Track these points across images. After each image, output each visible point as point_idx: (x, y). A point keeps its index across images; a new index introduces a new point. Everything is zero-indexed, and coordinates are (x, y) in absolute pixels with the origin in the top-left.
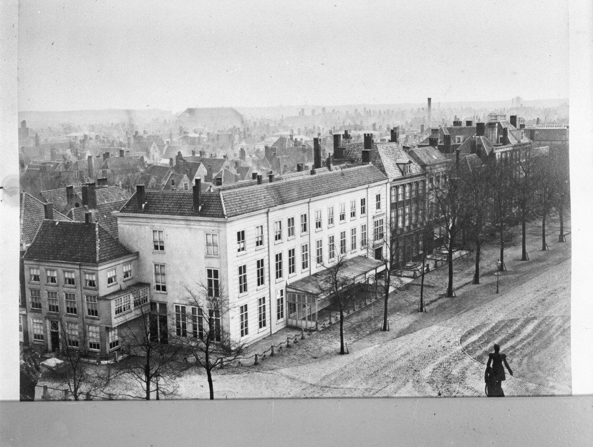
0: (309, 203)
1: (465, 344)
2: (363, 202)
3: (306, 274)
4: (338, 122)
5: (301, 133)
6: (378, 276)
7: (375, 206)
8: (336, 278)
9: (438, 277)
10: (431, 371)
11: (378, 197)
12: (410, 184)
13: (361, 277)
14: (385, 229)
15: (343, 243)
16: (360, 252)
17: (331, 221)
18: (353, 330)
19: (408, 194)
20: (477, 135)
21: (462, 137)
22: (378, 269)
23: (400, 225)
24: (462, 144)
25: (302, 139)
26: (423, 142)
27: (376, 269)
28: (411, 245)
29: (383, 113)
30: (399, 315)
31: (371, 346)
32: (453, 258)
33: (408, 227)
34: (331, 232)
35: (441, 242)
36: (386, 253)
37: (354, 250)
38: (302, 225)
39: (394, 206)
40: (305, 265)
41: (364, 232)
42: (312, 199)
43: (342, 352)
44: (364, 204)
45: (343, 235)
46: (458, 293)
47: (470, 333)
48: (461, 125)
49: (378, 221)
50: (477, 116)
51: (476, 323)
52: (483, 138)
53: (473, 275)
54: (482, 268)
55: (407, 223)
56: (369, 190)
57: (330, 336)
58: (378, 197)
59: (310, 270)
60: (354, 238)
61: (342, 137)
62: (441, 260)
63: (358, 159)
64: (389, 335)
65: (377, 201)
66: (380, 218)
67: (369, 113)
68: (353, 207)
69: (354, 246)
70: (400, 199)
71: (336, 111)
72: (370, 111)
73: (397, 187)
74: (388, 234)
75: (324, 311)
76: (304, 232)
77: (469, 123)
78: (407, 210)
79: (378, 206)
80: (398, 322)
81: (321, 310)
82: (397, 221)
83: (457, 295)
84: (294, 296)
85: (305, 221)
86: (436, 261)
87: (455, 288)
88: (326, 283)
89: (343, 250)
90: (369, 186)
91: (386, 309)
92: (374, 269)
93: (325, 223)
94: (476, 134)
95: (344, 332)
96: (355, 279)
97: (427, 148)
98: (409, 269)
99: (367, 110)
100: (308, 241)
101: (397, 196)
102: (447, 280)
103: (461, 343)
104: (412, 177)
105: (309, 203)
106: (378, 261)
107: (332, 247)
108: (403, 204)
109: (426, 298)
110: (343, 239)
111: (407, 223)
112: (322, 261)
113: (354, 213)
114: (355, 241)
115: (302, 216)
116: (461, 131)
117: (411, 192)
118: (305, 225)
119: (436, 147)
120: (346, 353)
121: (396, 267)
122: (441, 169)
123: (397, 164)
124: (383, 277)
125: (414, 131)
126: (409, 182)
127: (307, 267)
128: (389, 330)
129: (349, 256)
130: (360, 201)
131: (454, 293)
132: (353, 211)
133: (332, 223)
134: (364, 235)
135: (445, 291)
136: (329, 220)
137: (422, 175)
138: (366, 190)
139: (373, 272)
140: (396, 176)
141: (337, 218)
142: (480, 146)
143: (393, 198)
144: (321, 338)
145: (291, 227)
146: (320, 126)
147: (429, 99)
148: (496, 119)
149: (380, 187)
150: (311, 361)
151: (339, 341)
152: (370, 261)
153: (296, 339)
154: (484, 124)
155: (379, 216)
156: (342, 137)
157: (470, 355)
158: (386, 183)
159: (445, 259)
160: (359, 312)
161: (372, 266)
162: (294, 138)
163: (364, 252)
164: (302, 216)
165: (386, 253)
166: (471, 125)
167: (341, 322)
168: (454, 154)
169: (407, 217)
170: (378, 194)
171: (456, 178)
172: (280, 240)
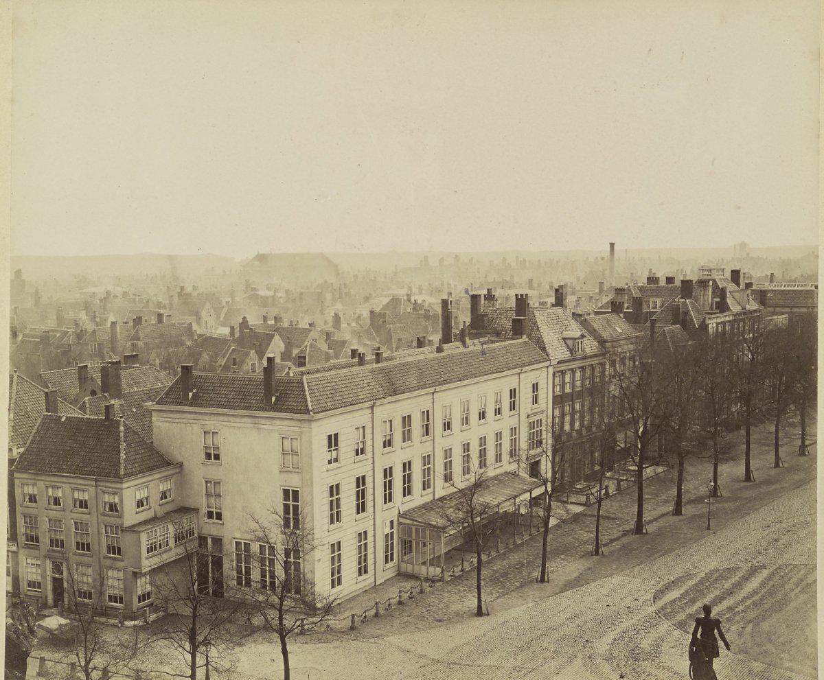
0: (433, 393)
1: (660, 604)
2: (513, 393)
3: (429, 498)
5: (423, 292)
6: (534, 502)
8: (471, 504)
10: (610, 642)
11: (535, 387)
12: (582, 368)
16: (507, 466)
17: (466, 420)
18: (496, 580)
19: (578, 383)
21: (659, 301)
23: (567, 427)
27: (530, 491)
34: (482, 431)
35: (626, 453)
39: (559, 400)
40: (426, 485)
42: (439, 388)
43: (480, 613)
45: (483, 441)
46: (650, 529)
47: (668, 588)
49: (534, 422)
51: (677, 572)
52: (691, 303)
55: (577, 425)
58: (535, 387)
60: (499, 446)
62: (627, 480)
65: (534, 392)
68: (498, 401)
69: (498, 458)
72: (525, 260)
73: (563, 373)
74: (548, 440)
75: (454, 552)
77: (670, 280)
78: (577, 407)
79: (535, 400)
80: (563, 569)
85: (428, 420)
86: (619, 481)
89: (483, 464)
92: (528, 491)
93: (474, 417)
96: (500, 507)
100: (432, 449)
101: (563, 386)
102: (636, 509)
104: (585, 358)
106: (534, 479)
107: (466, 458)
108: (571, 397)
111: (577, 425)
112: (451, 480)
113: (499, 409)
115: (423, 412)
116: (658, 292)
117: (583, 379)
118: (427, 425)
120: (485, 615)
121: (560, 490)
123: (563, 339)
127: (429, 487)
129: (491, 472)
131: (644, 528)
132: (498, 406)
134: (514, 442)
135: (631, 525)
136: (463, 419)
137: (600, 355)
139: (527, 496)
140: (562, 356)
141: (474, 417)
142: (686, 313)
143: (558, 389)
147: (612, 245)
148: (710, 275)
149: (538, 372)
151: (474, 596)
152: (523, 480)
156: (483, 298)
166: (673, 283)
169: (577, 416)
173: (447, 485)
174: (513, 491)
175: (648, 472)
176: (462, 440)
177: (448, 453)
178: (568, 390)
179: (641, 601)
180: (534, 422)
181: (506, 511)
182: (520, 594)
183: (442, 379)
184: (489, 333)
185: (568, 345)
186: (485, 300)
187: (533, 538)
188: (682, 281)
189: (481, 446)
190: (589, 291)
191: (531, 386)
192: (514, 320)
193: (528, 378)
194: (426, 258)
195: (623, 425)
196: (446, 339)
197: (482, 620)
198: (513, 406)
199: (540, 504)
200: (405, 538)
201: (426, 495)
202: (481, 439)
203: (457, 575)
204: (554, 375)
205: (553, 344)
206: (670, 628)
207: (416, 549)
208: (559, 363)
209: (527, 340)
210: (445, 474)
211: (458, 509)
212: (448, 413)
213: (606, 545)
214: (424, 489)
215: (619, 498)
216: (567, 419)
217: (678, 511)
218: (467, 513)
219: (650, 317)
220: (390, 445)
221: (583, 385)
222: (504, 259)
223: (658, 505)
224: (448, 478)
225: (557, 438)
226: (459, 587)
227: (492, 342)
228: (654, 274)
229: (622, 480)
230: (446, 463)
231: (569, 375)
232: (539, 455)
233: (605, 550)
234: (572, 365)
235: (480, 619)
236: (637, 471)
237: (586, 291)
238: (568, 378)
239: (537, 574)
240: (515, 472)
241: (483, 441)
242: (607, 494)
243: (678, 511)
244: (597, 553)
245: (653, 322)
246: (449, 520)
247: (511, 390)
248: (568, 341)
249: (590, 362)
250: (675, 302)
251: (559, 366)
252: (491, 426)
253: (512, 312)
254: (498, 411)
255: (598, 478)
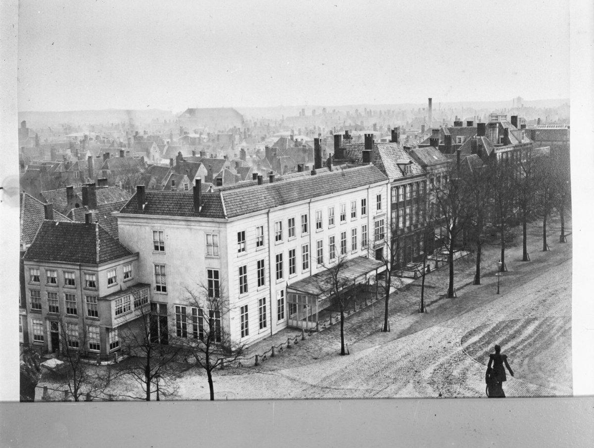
0: (309, 203)
1: (466, 345)
2: (364, 202)
3: (307, 275)
4: (339, 123)
5: (302, 133)
6: (379, 276)
7: (376, 207)
8: (336, 278)
9: (439, 277)
10: (432, 372)
11: (379, 198)
12: (411, 185)
13: (361, 278)
14: (385, 229)
15: (344, 244)
16: (360, 252)
17: (332, 221)
18: (353, 331)
19: (408, 195)
20: (478, 136)
21: (462, 138)
22: (378, 270)
23: (401, 225)
24: (463, 144)
25: (302, 139)
26: (424, 142)
27: (376, 269)
28: (411, 245)
29: (383, 113)
30: (399, 316)
31: (372, 347)
32: (454, 259)
33: (409, 228)
34: (331, 233)
35: (441, 242)
36: (387, 254)
37: (355, 251)
38: (303, 225)
39: (395, 207)
40: (305, 266)
41: (364, 232)
42: (313, 200)
43: (343, 353)
44: (365, 205)
45: (344, 235)
46: (458, 294)
47: (471, 334)
48: (462, 126)
49: (378, 222)
50: (478, 116)
51: (477, 323)
52: (484, 139)
53: (474, 276)
54: (482, 268)
55: (408, 224)
56: (370, 190)
57: (331, 337)
58: (379, 198)
59: (311, 271)
60: (354, 239)
61: (342, 137)
62: (442, 261)
63: (359, 159)
64: (390, 335)
65: (378, 201)
66: (381, 219)
67: (369, 113)
68: (354, 208)
69: (354, 247)
70: (401, 199)
71: (336, 111)
72: (370, 111)
73: (398, 188)
74: (388, 234)
75: (325, 312)
76: (305, 233)
77: (470, 123)
78: (408, 211)
79: (379, 207)
80: (399, 322)
81: (322, 311)
82: (398, 222)
83: (458, 296)
84: (295, 296)
85: (306, 222)
86: (437, 262)
87: (456, 288)
88: (326, 284)
89: (344, 251)
90: (369, 186)
91: (387, 310)
92: (375, 269)
93: (325, 224)
94: (476, 135)
95: (344, 333)
96: (356, 280)
97: (427, 148)
98: (410, 269)
99: (368, 110)
100: (309, 241)
101: (398, 196)
102: (448, 281)
103: (462, 344)
104: (412, 177)
105: (309, 203)
106: (379, 261)
107: (333, 247)
108: (404, 204)
109: (426, 298)
110: (344, 240)
111: (408, 224)
112: (322, 262)
113: (354, 213)
114: (356, 241)
115: (303, 216)
116: (462, 132)
117: (411, 192)
118: (305, 225)
119: (437, 148)
120: (346, 354)
121: (397, 268)
122: (441, 170)
123: (398, 164)
124: (383, 278)
125: (415, 131)
126: (409, 182)
127: (307, 267)
128: (389, 331)
129: (350, 257)
130: (361, 201)
131: (454, 294)
132: (354, 211)
133: (332, 223)
134: (365, 235)
135: (445, 291)
136: (330, 220)
137: (423, 175)
138: (366, 190)
139: (374, 273)
140: (397, 176)
141: (337, 218)
142: (481, 146)
143: (394, 199)
144: (321, 339)
145: (292, 227)
146: (320, 127)
147: (430, 100)
148: (497, 120)
149: (381, 187)
150: (311, 362)
151: (339, 342)
152: (371, 262)
153: (296, 340)
154: (485, 124)
155: (379, 216)
156: (342, 137)
157: (471, 356)
158: (387, 184)
159: (446, 260)
160: (359, 313)
161: (373, 267)
162: (294, 139)
163: (364, 253)
164: (303, 216)
165: (387, 254)
166: (472, 125)
167: (342, 323)
168: (455, 154)
169: (408, 217)
170: (378, 195)
171: (457, 179)
172: (281, 241)
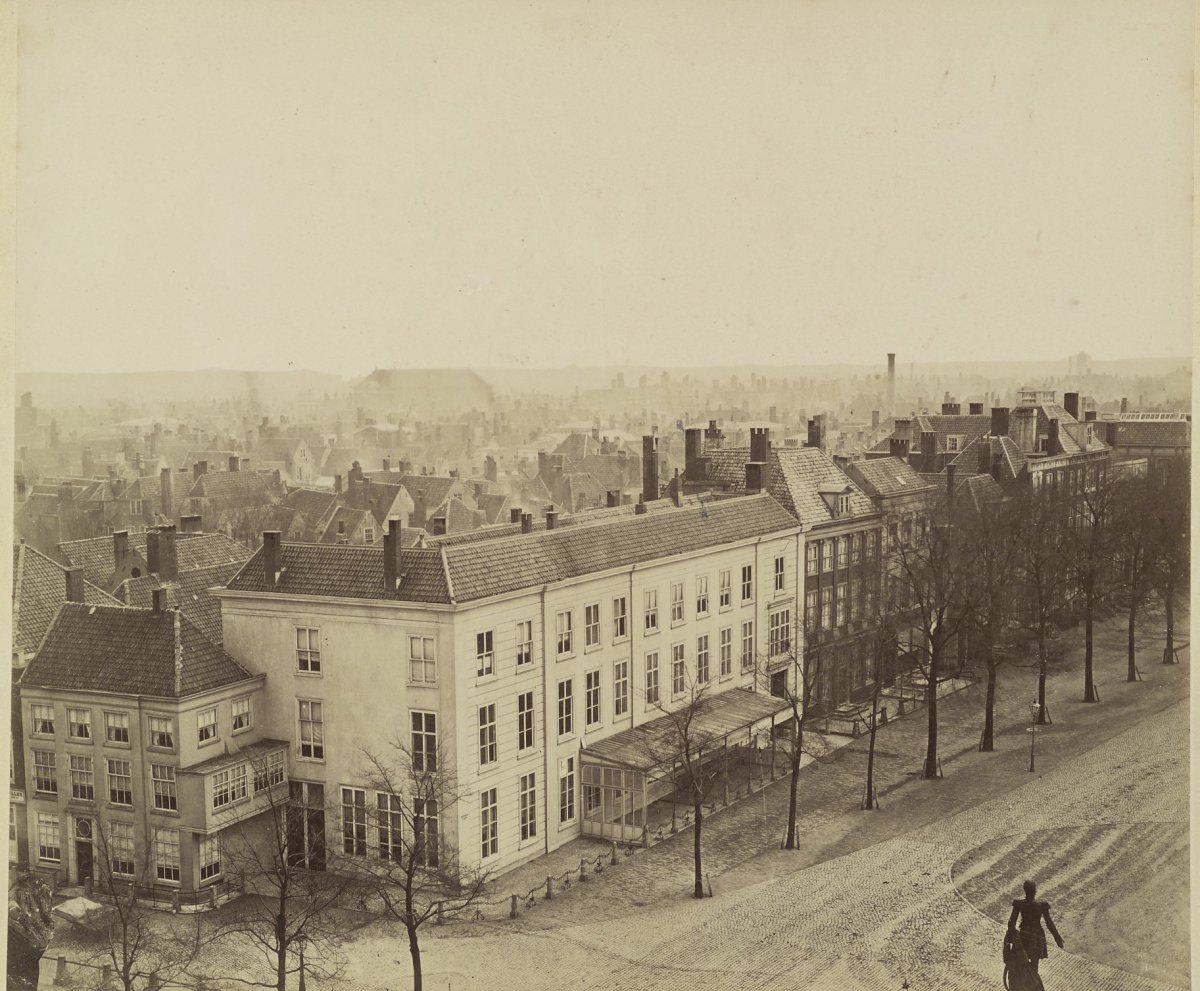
0: (631, 573)
1: (961, 880)
2: (747, 573)
3: (624, 726)
5: (617, 425)
6: (778, 731)
8: (686, 734)
10: (888, 936)
11: (779, 564)
12: (848, 537)
16: (739, 679)
17: (678, 613)
18: (722, 846)
19: (842, 559)
21: (959, 439)
23: (826, 623)
27: (772, 716)
34: (702, 629)
35: (912, 660)
39: (813, 583)
40: (620, 707)
42: (639, 566)
43: (698, 893)
45: (703, 642)
46: (947, 770)
47: (973, 856)
49: (777, 615)
51: (986, 834)
52: (1006, 441)
55: (840, 619)
58: (779, 564)
60: (726, 651)
62: (913, 699)
65: (777, 572)
68: (726, 584)
69: (726, 668)
72: (764, 379)
73: (820, 543)
74: (799, 642)
75: (661, 805)
77: (976, 408)
78: (841, 593)
79: (780, 583)
80: (820, 829)
85: (623, 612)
86: (902, 702)
89: (703, 676)
92: (768, 716)
93: (690, 607)
96: (729, 738)
100: (629, 655)
101: (820, 563)
102: (926, 742)
104: (852, 521)
106: (777, 699)
107: (679, 667)
108: (832, 579)
111: (840, 619)
112: (657, 699)
113: (727, 596)
115: (616, 601)
116: (958, 425)
117: (849, 552)
118: (622, 620)
120: (706, 896)
121: (816, 713)
123: (821, 493)
127: (625, 710)
129: (716, 688)
131: (938, 769)
132: (725, 592)
134: (748, 644)
135: (920, 765)
136: (674, 610)
137: (874, 517)
139: (767, 723)
140: (819, 519)
141: (690, 607)
142: (1000, 457)
143: (812, 567)
147: (891, 357)
148: (1035, 401)
149: (784, 542)
151: (691, 869)
152: (761, 700)
156: (703, 434)
166: (980, 412)
169: (840, 607)
173: (651, 706)
174: (746, 716)
175: (944, 687)
176: (673, 641)
177: (652, 660)
178: (827, 568)
179: (933, 875)
180: (777, 615)
181: (736, 745)
182: (757, 866)
183: (644, 553)
184: (712, 486)
185: (827, 503)
186: (706, 437)
187: (776, 784)
188: (994, 410)
189: (700, 650)
190: (858, 424)
191: (774, 562)
192: (749, 467)
193: (769, 551)
194: (620, 376)
195: (907, 620)
196: (650, 494)
197: (701, 904)
198: (747, 592)
199: (787, 735)
200: (590, 783)
201: (621, 721)
202: (700, 639)
203: (665, 838)
204: (807, 546)
205: (805, 502)
206: (976, 915)
207: (606, 800)
208: (814, 528)
209: (768, 495)
210: (649, 691)
211: (667, 742)
212: (652, 603)
213: (882, 794)
214: (618, 712)
215: (901, 725)
216: (826, 610)
217: (987, 745)
218: (680, 747)
219: (947, 461)
220: (567, 649)
221: (849, 561)
222: (734, 378)
223: (958, 735)
224: (652, 696)
225: (811, 638)
226: (668, 856)
227: (717, 498)
228: (953, 399)
229: (906, 700)
230: (649, 675)
231: (828, 547)
232: (785, 663)
233: (881, 801)
234: (833, 532)
235: (700, 901)
236: (928, 686)
237: (853, 424)
238: (827, 551)
239: (782, 836)
240: (750, 688)
241: (703, 642)
242: (884, 720)
243: (987, 745)
244: (869, 806)
245: (951, 469)
246: (654, 758)
247: (744, 569)
248: (827, 498)
249: (859, 527)
250: (982, 439)
251: (814, 533)
252: (715, 621)
253: (746, 455)
254: (725, 600)
255: (871, 696)
